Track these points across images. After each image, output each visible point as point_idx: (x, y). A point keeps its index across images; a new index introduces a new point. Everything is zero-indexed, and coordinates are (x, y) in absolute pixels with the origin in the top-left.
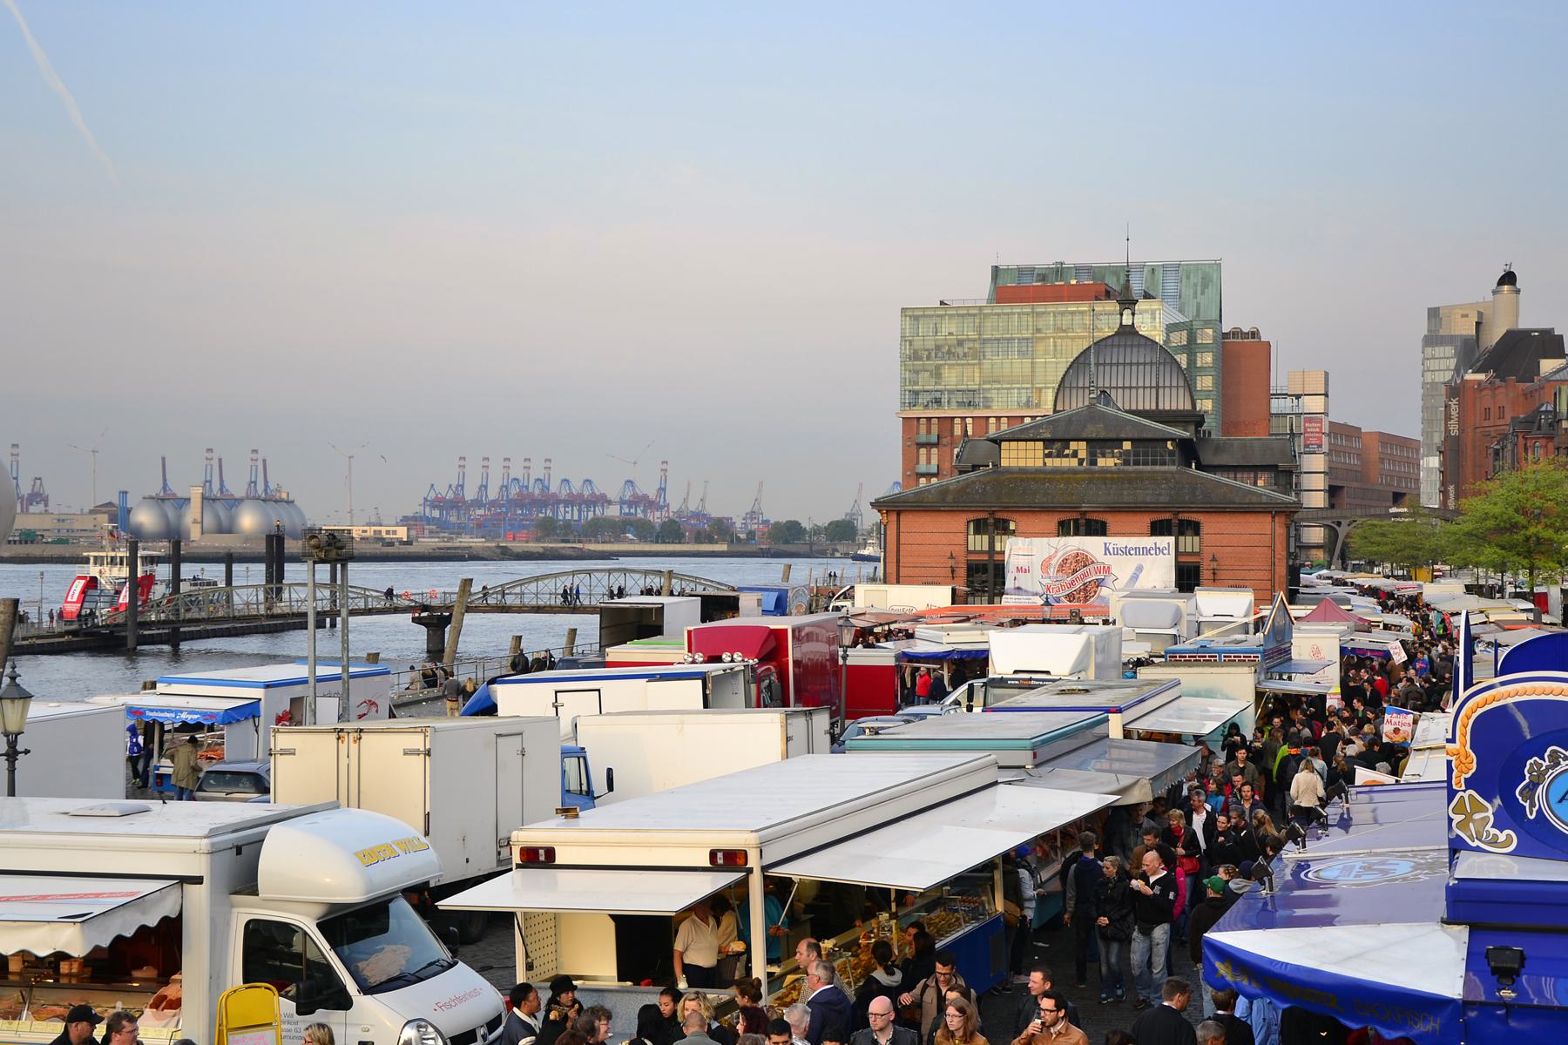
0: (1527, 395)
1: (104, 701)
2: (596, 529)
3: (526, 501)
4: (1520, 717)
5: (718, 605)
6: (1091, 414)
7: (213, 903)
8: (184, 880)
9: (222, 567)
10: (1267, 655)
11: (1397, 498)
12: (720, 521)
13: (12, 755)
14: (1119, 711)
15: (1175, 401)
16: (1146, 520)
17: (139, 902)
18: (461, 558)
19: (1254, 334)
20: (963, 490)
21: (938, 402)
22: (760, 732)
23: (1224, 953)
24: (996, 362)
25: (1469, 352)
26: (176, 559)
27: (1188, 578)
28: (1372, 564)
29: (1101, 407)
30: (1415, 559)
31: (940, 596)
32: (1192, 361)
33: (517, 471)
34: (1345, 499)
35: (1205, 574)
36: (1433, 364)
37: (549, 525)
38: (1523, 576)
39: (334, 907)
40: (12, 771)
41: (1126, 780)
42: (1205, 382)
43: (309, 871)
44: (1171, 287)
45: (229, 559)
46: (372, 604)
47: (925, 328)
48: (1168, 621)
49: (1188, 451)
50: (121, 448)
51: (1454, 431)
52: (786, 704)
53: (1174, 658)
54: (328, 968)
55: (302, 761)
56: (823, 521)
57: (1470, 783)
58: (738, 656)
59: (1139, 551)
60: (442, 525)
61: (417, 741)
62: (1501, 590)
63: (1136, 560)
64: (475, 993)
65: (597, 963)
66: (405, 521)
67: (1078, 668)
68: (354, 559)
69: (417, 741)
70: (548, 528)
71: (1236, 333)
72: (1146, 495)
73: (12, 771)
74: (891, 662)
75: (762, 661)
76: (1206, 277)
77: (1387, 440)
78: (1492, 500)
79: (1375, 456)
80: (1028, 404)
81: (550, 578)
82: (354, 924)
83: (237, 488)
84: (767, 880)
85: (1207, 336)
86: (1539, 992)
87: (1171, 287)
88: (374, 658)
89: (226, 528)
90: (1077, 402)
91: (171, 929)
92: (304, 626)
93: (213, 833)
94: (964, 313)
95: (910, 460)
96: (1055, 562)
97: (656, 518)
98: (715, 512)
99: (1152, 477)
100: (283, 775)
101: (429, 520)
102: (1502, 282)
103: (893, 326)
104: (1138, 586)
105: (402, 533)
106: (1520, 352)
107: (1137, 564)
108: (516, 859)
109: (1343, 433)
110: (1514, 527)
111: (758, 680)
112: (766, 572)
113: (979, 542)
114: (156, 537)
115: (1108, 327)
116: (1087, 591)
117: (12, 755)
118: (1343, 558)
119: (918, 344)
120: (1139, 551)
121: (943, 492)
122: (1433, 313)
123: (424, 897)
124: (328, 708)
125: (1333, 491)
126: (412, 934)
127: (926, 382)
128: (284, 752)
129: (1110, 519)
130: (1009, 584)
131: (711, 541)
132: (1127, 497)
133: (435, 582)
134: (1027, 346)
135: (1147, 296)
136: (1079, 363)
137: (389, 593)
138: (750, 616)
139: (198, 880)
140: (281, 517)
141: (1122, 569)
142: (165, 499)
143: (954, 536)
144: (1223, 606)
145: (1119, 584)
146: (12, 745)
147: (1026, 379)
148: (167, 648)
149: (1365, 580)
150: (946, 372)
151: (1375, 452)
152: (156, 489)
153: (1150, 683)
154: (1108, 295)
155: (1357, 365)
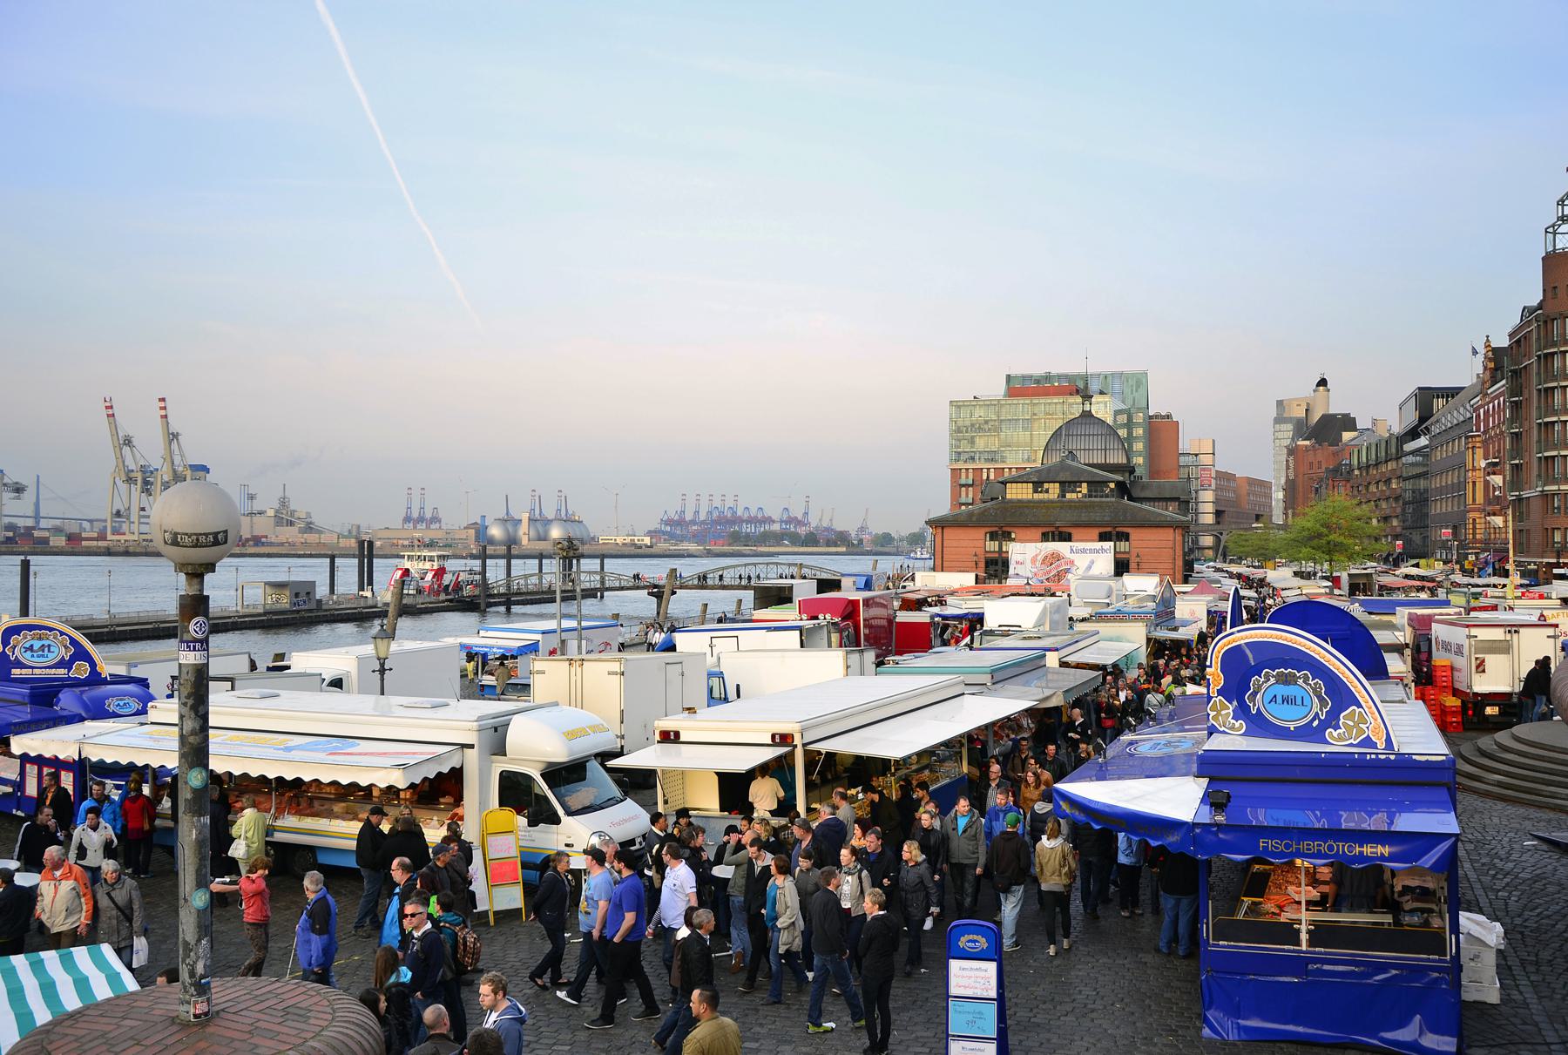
0: (1335, 454)
1: (450, 641)
2: (765, 538)
5: (825, 585)
6: (1062, 466)
7: (480, 760)
8: (463, 746)
9: (598, 561)
10: (1158, 615)
11: (1258, 518)
12: (841, 532)
13: (382, 671)
14: (1056, 650)
15: (1117, 458)
16: (1096, 532)
17: (436, 758)
18: (683, 556)
19: (1169, 416)
21: (973, 459)
22: (829, 661)
23: (1065, 797)
24: (1007, 433)
25: (1303, 428)
26: (509, 557)
27: (1121, 567)
28: (1241, 559)
29: (1069, 462)
30: (1266, 556)
31: (968, 579)
32: (1130, 433)
33: (717, 503)
34: (1226, 517)
35: (1133, 565)
36: (1280, 435)
37: (733, 533)
38: (1326, 566)
39: (550, 764)
40: (382, 680)
41: (1048, 693)
42: (1139, 446)
43: (537, 741)
45: (541, 557)
46: (624, 584)
47: (965, 413)
48: (1104, 594)
49: (1122, 489)
50: (18, 511)
53: (1099, 617)
54: (546, 798)
55: (548, 676)
56: (905, 533)
57: (1220, 693)
58: (828, 616)
59: (1091, 551)
60: (672, 536)
61: (616, 667)
62: (1315, 574)
63: (1088, 558)
64: (636, 817)
65: (707, 800)
66: (650, 533)
67: (1039, 624)
68: (583, 556)
69: (616, 667)
70: (736, 538)
72: (1096, 516)
73: (382, 680)
74: (928, 620)
75: (844, 619)
77: (1252, 482)
78: (1308, 520)
79: (1244, 492)
80: (1028, 460)
81: (732, 568)
82: (565, 774)
83: (550, 513)
84: (807, 753)
85: (1139, 418)
86: (1257, 819)
87: (1117, 387)
88: (616, 616)
89: (543, 538)
90: (1055, 459)
91: (457, 775)
92: (553, 601)
93: (480, 719)
94: (989, 404)
95: (955, 495)
96: (1040, 558)
97: (802, 531)
98: (839, 526)
99: (1100, 505)
100: (537, 683)
101: (664, 533)
102: (1319, 384)
103: (1273, 412)
104: (1091, 573)
105: (647, 541)
106: (1329, 428)
107: (1090, 559)
108: (657, 737)
109: (1223, 477)
110: (1320, 536)
111: (841, 631)
112: (863, 565)
113: (993, 546)
115: (1076, 412)
116: (1060, 576)
117: (382, 671)
118: (1225, 556)
119: (960, 423)
120: (1091, 551)
121: (971, 514)
122: (1280, 403)
123: (604, 757)
124: (572, 645)
125: (1218, 514)
126: (600, 782)
127: (965, 447)
128: (539, 672)
129: (1073, 531)
130: (1011, 571)
132: (1084, 518)
133: (655, 571)
134: (1028, 424)
135: (1102, 393)
136: (1056, 435)
137: (636, 577)
138: (849, 592)
139: (472, 746)
140: (575, 532)
141: (1081, 562)
142: (509, 521)
143: (979, 543)
144: (1142, 585)
145: (1080, 572)
146: (382, 665)
147: (1025, 444)
148: (502, 609)
149: (1235, 569)
150: (977, 440)
152: (503, 515)
153: (1080, 633)
154: (1078, 392)
155: (1234, 436)
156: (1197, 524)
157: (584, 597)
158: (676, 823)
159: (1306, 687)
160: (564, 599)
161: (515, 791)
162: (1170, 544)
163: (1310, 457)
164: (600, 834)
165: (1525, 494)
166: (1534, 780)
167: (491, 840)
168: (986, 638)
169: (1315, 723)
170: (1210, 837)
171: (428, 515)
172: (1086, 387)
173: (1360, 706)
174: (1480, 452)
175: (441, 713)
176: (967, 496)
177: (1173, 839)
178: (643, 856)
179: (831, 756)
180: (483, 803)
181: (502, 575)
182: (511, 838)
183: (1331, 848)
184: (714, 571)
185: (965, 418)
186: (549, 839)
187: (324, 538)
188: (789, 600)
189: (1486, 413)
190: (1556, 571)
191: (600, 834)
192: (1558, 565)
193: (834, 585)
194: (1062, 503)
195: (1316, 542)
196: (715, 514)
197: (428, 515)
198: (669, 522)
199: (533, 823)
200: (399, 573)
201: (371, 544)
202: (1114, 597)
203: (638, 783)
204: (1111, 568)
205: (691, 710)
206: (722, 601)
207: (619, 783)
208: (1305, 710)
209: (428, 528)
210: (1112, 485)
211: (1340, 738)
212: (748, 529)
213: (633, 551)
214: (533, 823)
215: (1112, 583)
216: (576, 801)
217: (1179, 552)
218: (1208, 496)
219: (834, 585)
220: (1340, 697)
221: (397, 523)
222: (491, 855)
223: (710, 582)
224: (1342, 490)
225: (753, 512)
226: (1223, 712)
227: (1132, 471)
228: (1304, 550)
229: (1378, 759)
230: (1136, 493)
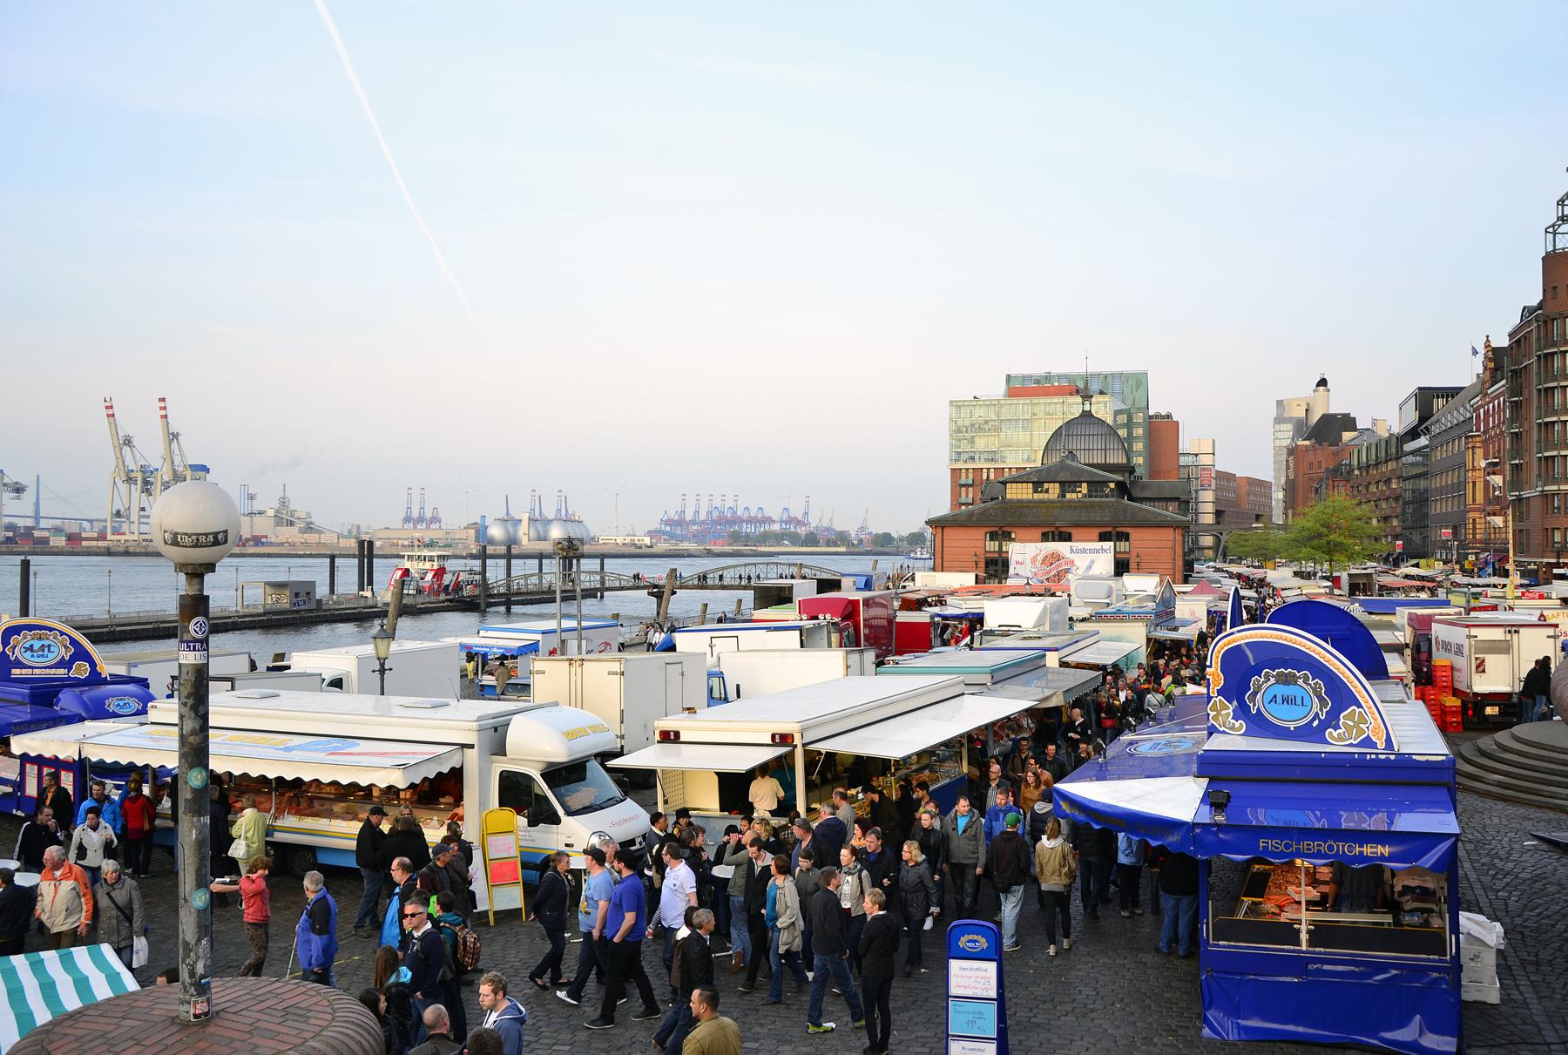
0: (1335, 454)
1: (450, 641)
2: (765, 538)
3: (723, 521)
4: (1248, 652)
5: (825, 585)
6: (1062, 466)
7: (480, 760)
8: (463, 746)
9: (598, 561)
10: (1158, 615)
11: (1258, 518)
12: (841, 533)
13: (382, 671)
15: (1117, 458)
16: (1096, 532)
17: (436, 758)
18: (683, 556)
19: (1169, 416)
20: (984, 512)
21: (973, 459)
22: (829, 661)
23: (1065, 797)
24: (1008, 434)
25: (1301, 427)
26: (509, 556)
27: (1121, 567)
28: (1241, 559)
29: (1069, 462)
30: (1266, 556)
31: (968, 579)
32: (1130, 433)
34: (1226, 517)
35: (1133, 565)
36: (1280, 435)
37: (737, 536)
38: (1326, 566)
40: (382, 680)
41: (1048, 693)
42: (1139, 446)
43: (537, 741)
44: (1117, 387)
45: (541, 557)
46: (624, 584)
47: (965, 413)
49: (1122, 489)
51: (1292, 477)
52: (858, 645)
53: (1099, 617)
54: (546, 798)
55: (548, 676)
56: (905, 533)
57: (1220, 693)
58: (828, 616)
59: (1092, 551)
60: (672, 536)
61: (616, 667)
62: (1315, 574)
63: (1088, 557)
64: (636, 817)
65: (707, 800)
67: (1039, 624)
68: (583, 556)
69: (616, 667)
70: (736, 537)
71: (1157, 416)
72: (1096, 516)
73: (382, 680)
75: (844, 619)
76: (1139, 381)
77: (1252, 482)
78: (1308, 520)
79: (1244, 492)
80: (1028, 460)
81: (733, 569)
82: (565, 774)
83: (550, 513)
84: (807, 753)
86: (1257, 819)
87: (1117, 387)
90: (1055, 459)
91: (457, 775)
93: (480, 719)
94: (989, 404)
95: (955, 495)
96: (1040, 558)
97: (802, 531)
98: (839, 527)
99: (1100, 505)
100: (537, 683)
101: (664, 533)
102: (1319, 385)
103: (945, 411)
104: (1091, 573)
105: (647, 541)
106: (1331, 427)
107: (1090, 559)
108: (657, 737)
109: (1224, 477)
110: (1320, 536)
111: (841, 631)
112: (864, 565)
113: (993, 546)
114: (501, 543)
115: (1076, 412)
116: (1060, 576)
117: (382, 671)
118: (1225, 556)
119: (960, 423)
120: (1092, 551)
121: (971, 514)
122: (1280, 403)
123: (604, 757)
124: (572, 645)
125: (1218, 514)
126: (600, 782)
128: (539, 672)
129: (1073, 531)
130: (1011, 572)
131: (836, 545)
132: (1084, 518)
133: (656, 571)
134: (1028, 424)
135: (1102, 393)
136: (1056, 435)
137: (636, 577)
138: (849, 592)
139: (472, 746)
140: (575, 532)
141: (1081, 561)
142: (509, 521)
143: (979, 543)
144: (1142, 585)
145: (1080, 572)
146: (382, 665)
147: (1024, 445)
148: (502, 609)
149: (1235, 569)
150: (977, 440)
151: (1245, 488)
152: (502, 514)
153: (1080, 633)
154: (1078, 392)
155: (1234, 435)
156: (1197, 524)
157: (584, 597)
158: (676, 823)
159: (1306, 687)
160: (564, 599)
161: (515, 791)
162: (1170, 544)
163: (1310, 457)
164: (600, 834)
165: (1525, 494)
166: (1534, 780)
167: (491, 840)
168: (986, 638)
169: (1315, 723)
170: (1210, 837)
171: (428, 515)
172: (1086, 387)
173: (1360, 706)
174: (1480, 452)
175: (440, 713)
176: (968, 495)
177: (1173, 839)
178: (643, 856)
179: (831, 756)
180: (483, 803)
181: (502, 575)
182: (511, 838)
183: (1331, 848)
184: (714, 571)
185: (965, 418)
186: (549, 839)
187: (324, 538)
188: (789, 600)
189: (1486, 413)
190: (1556, 571)
191: (600, 834)
192: (1558, 565)
193: (834, 585)
194: (1061, 503)
195: (1316, 542)
196: (715, 514)
197: (428, 515)
198: (669, 522)
199: (533, 823)
200: (399, 573)
201: (371, 544)
202: (1114, 597)
203: (638, 783)
204: (1111, 568)
205: (691, 710)
206: (722, 601)
207: (619, 783)
208: (1305, 710)
209: (428, 527)
210: (1112, 485)
211: (1340, 738)
212: (748, 529)
213: (633, 550)
214: (533, 823)
215: (1112, 583)
216: (576, 801)
217: (1179, 552)
218: (1208, 496)
219: (834, 585)
220: (1340, 697)
221: (397, 523)
222: (492, 854)
223: (710, 582)
224: (1342, 490)
225: (753, 512)
226: (1223, 712)
227: (1132, 471)
228: (1304, 550)
229: (1378, 759)
230: (1136, 493)
